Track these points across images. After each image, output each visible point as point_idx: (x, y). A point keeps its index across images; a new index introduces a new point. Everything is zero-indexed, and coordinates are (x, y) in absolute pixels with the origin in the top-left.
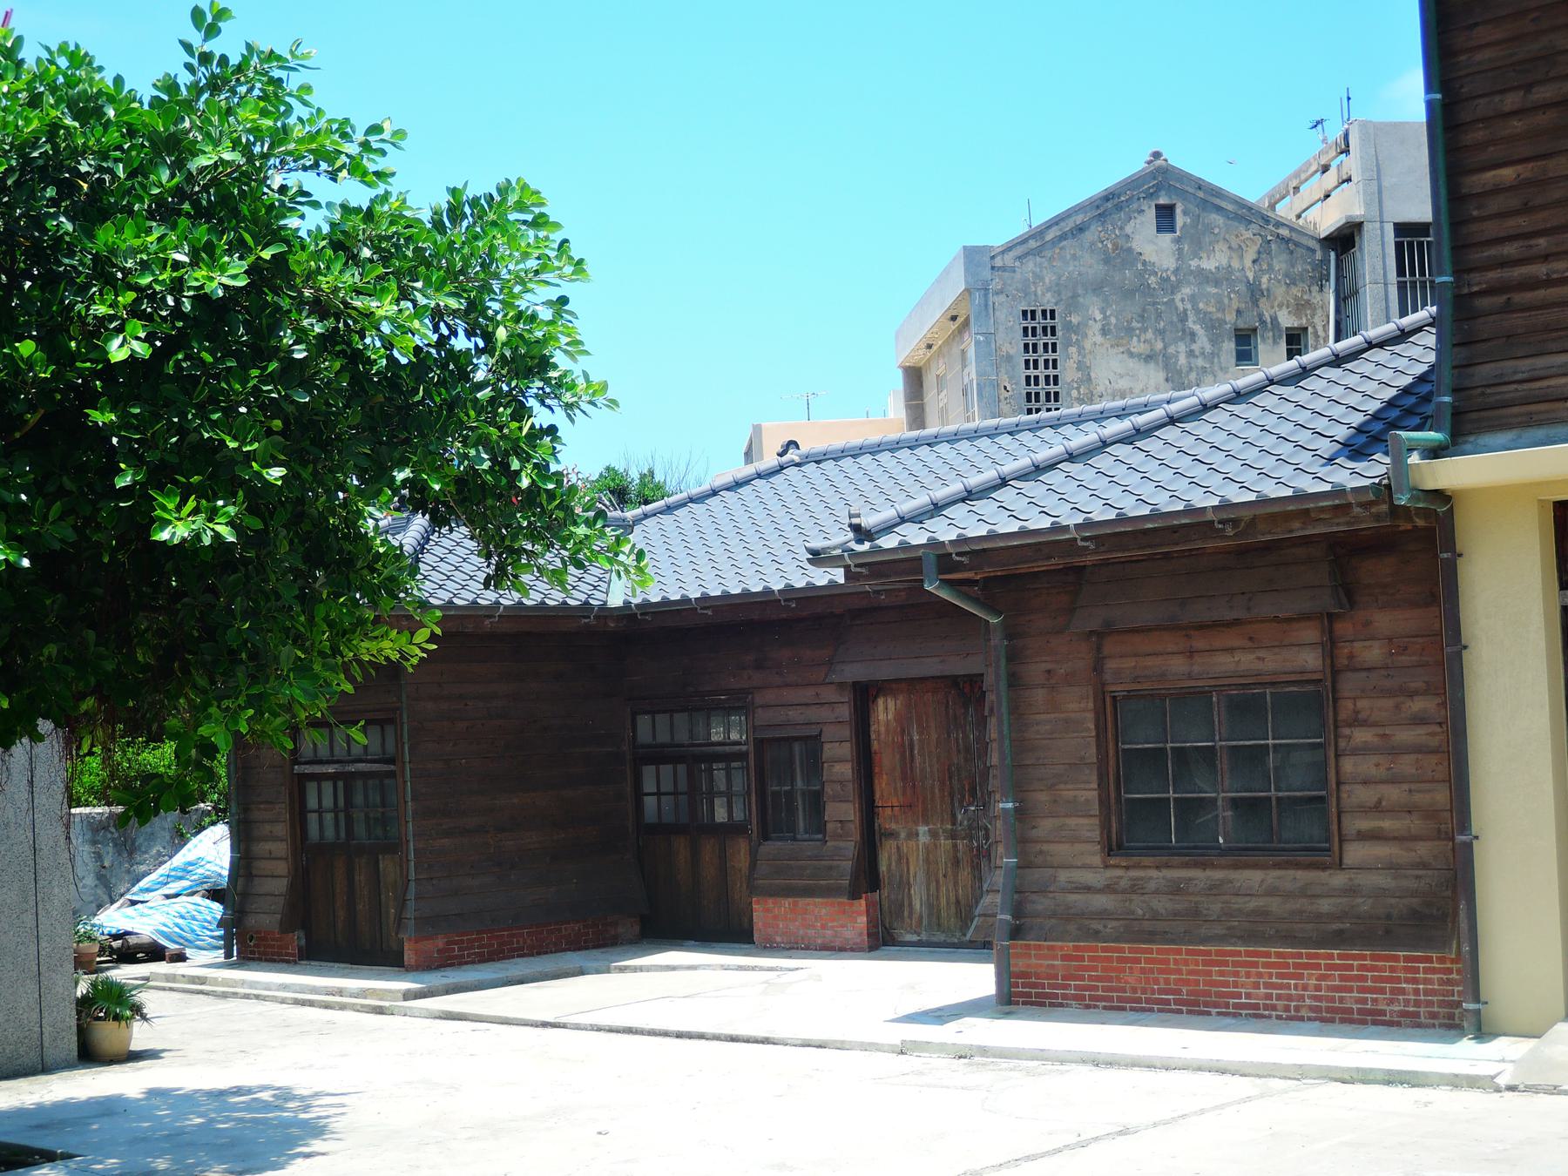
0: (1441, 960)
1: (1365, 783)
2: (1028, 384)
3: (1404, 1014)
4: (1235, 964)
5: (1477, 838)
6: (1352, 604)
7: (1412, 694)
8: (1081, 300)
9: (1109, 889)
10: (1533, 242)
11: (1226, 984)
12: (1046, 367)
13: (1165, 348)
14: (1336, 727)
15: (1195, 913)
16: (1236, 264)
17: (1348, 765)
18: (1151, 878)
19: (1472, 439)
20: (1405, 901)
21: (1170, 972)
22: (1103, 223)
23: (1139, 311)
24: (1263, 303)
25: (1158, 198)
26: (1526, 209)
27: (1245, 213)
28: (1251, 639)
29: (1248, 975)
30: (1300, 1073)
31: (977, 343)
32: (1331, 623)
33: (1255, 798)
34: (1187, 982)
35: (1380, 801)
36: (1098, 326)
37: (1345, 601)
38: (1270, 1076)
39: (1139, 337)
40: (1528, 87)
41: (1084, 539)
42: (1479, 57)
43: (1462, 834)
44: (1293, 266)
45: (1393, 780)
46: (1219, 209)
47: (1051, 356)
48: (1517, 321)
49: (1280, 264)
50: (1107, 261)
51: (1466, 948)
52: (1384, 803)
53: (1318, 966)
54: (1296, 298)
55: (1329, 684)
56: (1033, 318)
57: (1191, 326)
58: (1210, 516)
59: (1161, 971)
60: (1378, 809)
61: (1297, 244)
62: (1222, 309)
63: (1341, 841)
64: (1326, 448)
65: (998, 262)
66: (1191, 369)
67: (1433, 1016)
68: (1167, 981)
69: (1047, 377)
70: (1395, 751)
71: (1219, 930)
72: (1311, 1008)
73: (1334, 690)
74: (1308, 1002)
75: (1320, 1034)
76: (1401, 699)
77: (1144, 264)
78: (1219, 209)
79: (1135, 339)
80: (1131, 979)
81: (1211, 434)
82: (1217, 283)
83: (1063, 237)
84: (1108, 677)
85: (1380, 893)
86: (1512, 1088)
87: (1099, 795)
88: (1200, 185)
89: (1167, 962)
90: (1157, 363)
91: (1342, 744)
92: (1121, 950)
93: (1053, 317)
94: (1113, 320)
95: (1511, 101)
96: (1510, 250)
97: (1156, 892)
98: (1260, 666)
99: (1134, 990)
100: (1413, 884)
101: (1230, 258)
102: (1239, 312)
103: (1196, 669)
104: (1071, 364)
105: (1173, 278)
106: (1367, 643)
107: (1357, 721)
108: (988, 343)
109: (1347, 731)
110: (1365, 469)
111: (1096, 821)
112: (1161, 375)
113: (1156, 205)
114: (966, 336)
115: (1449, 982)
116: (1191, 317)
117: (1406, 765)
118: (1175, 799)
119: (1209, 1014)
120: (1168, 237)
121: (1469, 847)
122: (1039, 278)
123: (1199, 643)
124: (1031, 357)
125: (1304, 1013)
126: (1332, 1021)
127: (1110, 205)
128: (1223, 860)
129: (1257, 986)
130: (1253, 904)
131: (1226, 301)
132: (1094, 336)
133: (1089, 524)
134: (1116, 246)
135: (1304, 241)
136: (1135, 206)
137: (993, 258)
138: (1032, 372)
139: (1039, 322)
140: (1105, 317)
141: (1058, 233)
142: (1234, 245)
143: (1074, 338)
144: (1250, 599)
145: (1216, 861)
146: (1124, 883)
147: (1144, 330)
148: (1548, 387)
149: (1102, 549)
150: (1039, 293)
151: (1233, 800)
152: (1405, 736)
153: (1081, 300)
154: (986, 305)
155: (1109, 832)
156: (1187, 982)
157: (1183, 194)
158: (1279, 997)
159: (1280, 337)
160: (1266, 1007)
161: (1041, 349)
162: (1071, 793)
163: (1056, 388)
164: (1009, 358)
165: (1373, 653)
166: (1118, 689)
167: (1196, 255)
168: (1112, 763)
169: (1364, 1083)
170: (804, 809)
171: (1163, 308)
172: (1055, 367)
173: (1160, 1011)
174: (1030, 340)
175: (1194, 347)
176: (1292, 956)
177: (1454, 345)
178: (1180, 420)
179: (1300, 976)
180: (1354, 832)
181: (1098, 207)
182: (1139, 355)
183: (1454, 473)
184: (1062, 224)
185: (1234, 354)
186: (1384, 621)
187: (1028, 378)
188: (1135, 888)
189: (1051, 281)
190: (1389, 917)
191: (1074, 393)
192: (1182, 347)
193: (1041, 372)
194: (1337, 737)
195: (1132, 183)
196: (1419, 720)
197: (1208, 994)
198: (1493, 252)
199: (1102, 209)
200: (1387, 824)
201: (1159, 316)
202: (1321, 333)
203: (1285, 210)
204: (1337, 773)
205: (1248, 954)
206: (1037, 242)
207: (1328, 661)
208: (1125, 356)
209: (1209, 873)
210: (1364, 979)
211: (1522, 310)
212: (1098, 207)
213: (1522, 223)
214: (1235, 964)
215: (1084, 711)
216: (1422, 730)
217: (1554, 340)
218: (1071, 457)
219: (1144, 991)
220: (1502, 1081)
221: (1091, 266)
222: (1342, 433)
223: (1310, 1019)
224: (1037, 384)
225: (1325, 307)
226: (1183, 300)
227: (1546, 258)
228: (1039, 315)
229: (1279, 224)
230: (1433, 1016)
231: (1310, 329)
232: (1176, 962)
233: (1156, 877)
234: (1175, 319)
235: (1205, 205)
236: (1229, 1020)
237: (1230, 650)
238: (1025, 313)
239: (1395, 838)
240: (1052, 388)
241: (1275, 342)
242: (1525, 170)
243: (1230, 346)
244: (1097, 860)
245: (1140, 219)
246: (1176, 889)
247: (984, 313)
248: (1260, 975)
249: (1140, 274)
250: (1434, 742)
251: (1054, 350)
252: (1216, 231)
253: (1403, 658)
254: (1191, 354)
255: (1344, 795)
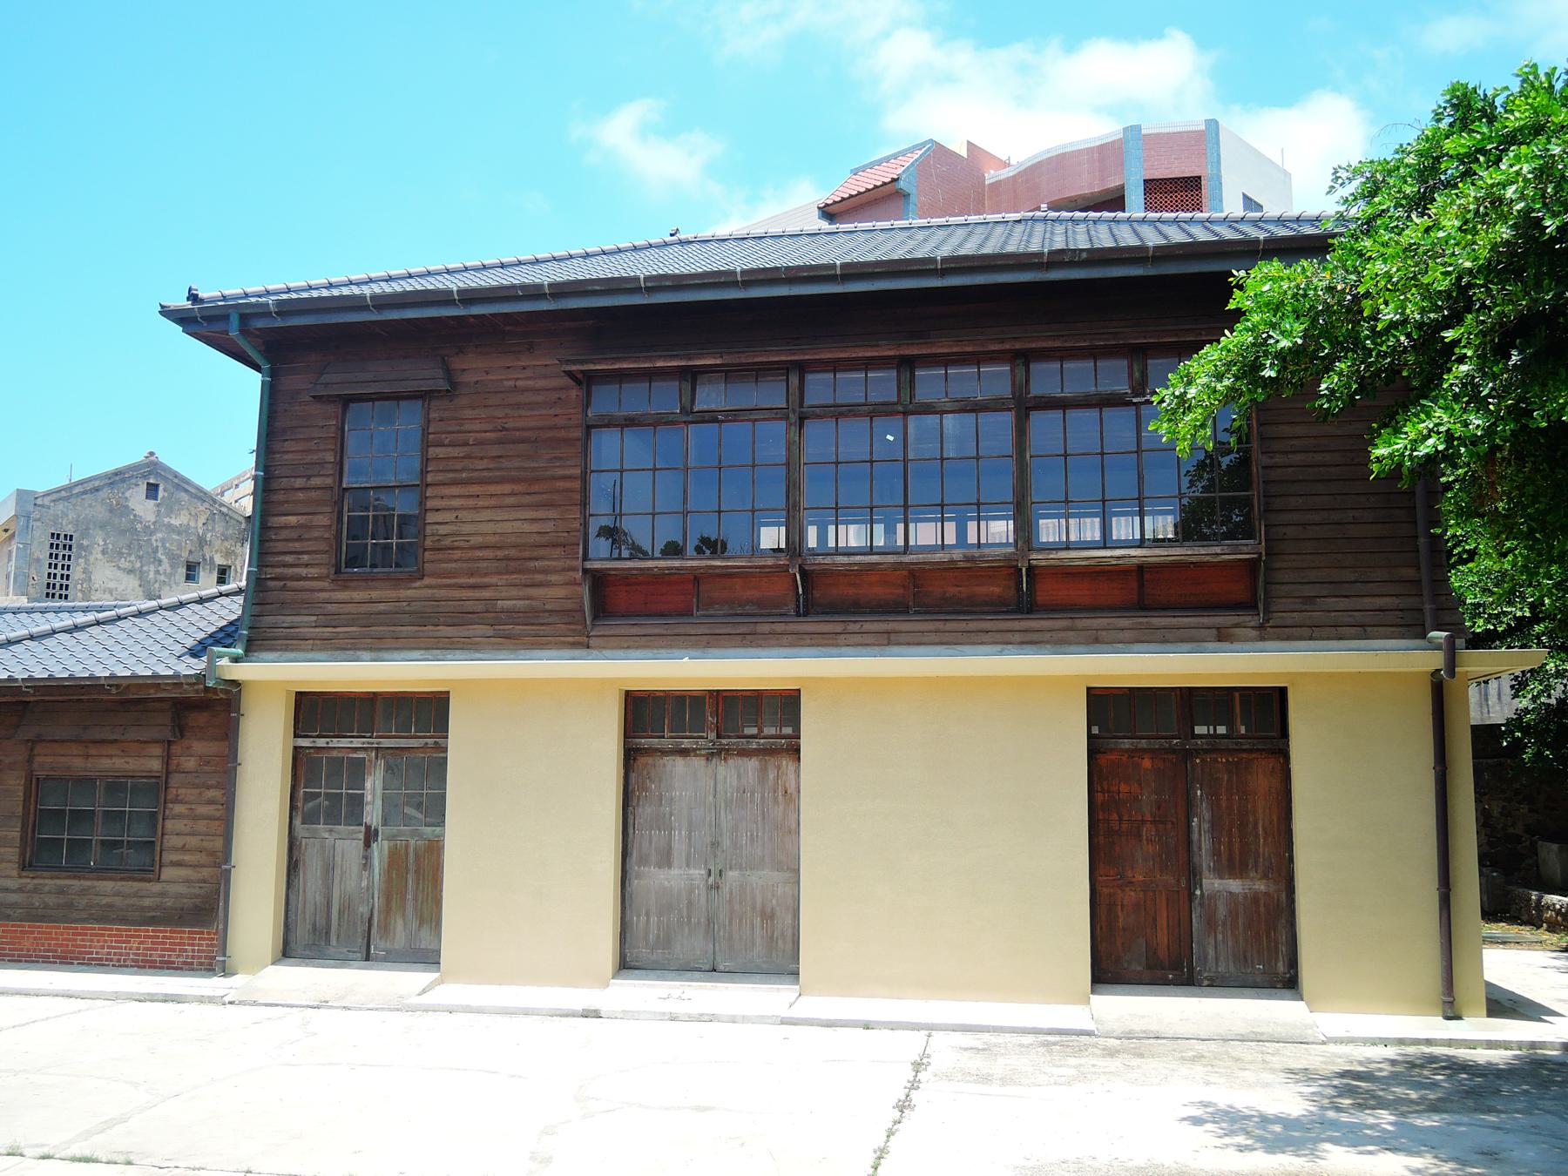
0: (208, 933)
1: (177, 834)
2: (49, 577)
3: (185, 963)
4: (92, 935)
5: (234, 867)
6: (182, 736)
7: (209, 787)
8: (91, 531)
9: (20, 890)
10: (300, 557)
11: (85, 947)
12: (63, 569)
13: (142, 566)
14: (165, 803)
15: (70, 906)
16: (192, 524)
17: (169, 824)
18: (46, 885)
19: (256, 654)
20: (192, 900)
21: (52, 939)
22: (112, 488)
23: (129, 543)
24: (206, 548)
25: (149, 479)
26: (299, 539)
27: (201, 495)
28: (123, 751)
29: (98, 941)
30: (116, 997)
31: (18, 548)
32: (169, 745)
33: (115, 840)
34: (61, 945)
35: (185, 845)
36: (101, 549)
37: (178, 734)
38: (98, 998)
39: (126, 558)
40: (309, 477)
41: (26, 687)
42: (286, 457)
43: (225, 864)
44: (227, 530)
45: (193, 834)
46: (186, 491)
47: (66, 562)
48: (288, 596)
49: (219, 527)
50: (111, 511)
51: (221, 927)
52: (187, 846)
53: (139, 936)
54: (226, 548)
55: (164, 779)
56: (58, 538)
57: (160, 556)
58: (102, 682)
59: (46, 939)
60: (183, 849)
61: (231, 518)
62: (180, 548)
63: (160, 866)
64: (178, 649)
65: (39, 502)
66: (156, 581)
67: (201, 964)
68: (49, 945)
69: (62, 575)
70: (197, 818)
71: (84, 915)
72: (133, 960)
73: (166, 782)
74: (131, 957)
75: (136, 974)
76: (202, 790)
77: (135, 516)
78: (186, 491)
79: (123, 559)
80: (27, 944)
81: (160, 622)
82: (179, 533)
83: (85, 493)
84: (35, 766)
85: (179, 896)
86: (231, 1003)
87: (21, 836)
88: (176, 475)
89: (50, 933)
90: (135, 575)
91: (167, 812)
92: (23, 926)
93: (71, 540)
94: (110, 546)
95: (299, 483)
96: (289, 559)
97: (49, 892)
98: (127, 766)
99: (28, 950)
100: (197, 891)
101: (190, 520)
102: (190, 552)
103: (89, 765)
104: (79, 569)
105: (152, 527)
106: (189, 758)
107: (177, 801)
108: (25, 549)
109: (171, 806)
110: (195, 664)
111: (17, 850)
112: (137, 583)
113: (148, 483)
114: (13, 543)
115: (212, 945)
116: (161, 551)
117: (201, 826)
118: (68, 839)
119: (72, 964)
120: (153, 502)
121: (229, 872)
122: (65, 515)
123: (93, 751)
124: (54, 561)
125: (128, 963)
126: (144, 967)
127: (118, 478)
128: (92, 875)
129: (103, 947)
130: (105, 901)
131: (184, 544)
132: (97, 554)
133: (31, 679)
134: (118, 504)
135: (236, 516)
136: (133, 481)
137: (36, 498)
138: (53, 571)
139: (62, 541)
140: (106, 544)
141: (82, 490)
142: (193, 513)
143: (84, 554)
144: (125, 729)
145: (87, 875)
146: (30, 887)
147: (130, 555)
148: (299, 632)
149: (38, 694)
150: (64, 523)
151: (102, 840)
152: (203, 810)
153: (91, 531)
154: (27, 527)
155: (25, 857)
156: (61, 945)
157: (166, 479)
158: (115, 954)
159: (214, 569)
160: (107, 960)
161: (60, 557)
162: (5, 833)
163: (67, 583)
164: (38, 560)
165: (190, 763)
166: (41, 773)
167: (168, 516)
168: (32, 816)
169: (152, 1001)
170: (525, 630)
171: (144, 543)
172: (68, 569)
173: (43, 962)
174: (54, 551)
175: (160, 568)
176: (126, 930)
177: (253, 604)
178: (103, 623)
179: (129, 942)
180: (168, 861)
181: (110, 478)
182: (124, 570)
183: (244, 672)
184: (85, 485)
185: (185, 575)
186: (199, 747)
187: (49, 574)
188: (36, 890)
189: (73, 518)
190: (182, 909)
191: (79, 587)
192: (152, 568)
193: (59, 571)
194: (165, 808)
195: (134, 468)
196: (211, 802)
197: (73, 952)
198: (280, 558)
199: (112, 480)
200: (187, 858)
201: (140, 547)
202: (239, 570)
203: (228, 498)
204: (163, 828)
205: (99, 929)
206: (68, 494)
207: (165, 767)
208: (116, 568)
209: (82, 882)
210: (165, 943)
211: (292, 591)
212: (110, 478)
213: (297, 546)
214: (92, 935)
215: (19, 785)
216: (213, 807)
217: (305, 608)
218: (32, 638)
219: (35, 950)
220: (227, 999)
221: (100, 512)
222: (190, 643)
223: (132, 966)
224: (55, 578)
225: (243, 555)
226: (156, 540)
227: (307, 565)
228: (62, 537)
229: (222, 505)
230: (201, 964)
231: (233, 567)
232: (56, 933)
233: (50, 883)
234: (150, 550)
235: (178, 487)
236: (84, 967)
237: (110, 756)
238: (53, 534)
239: (191, 866)
240: (65, 582)
241: (210, 572)
242: (302, 519)
243: (183, 571)
244: (15, 873)
245: (136, 489)
246: (61, 891)
247: (25, 531)
248: (106, 941)
249: (132, 522)
250: (218, 814)
251: (69, 559)
252: (183, 503)
253: (206, 768)
254: (157, 572)
255: (165, 841)
